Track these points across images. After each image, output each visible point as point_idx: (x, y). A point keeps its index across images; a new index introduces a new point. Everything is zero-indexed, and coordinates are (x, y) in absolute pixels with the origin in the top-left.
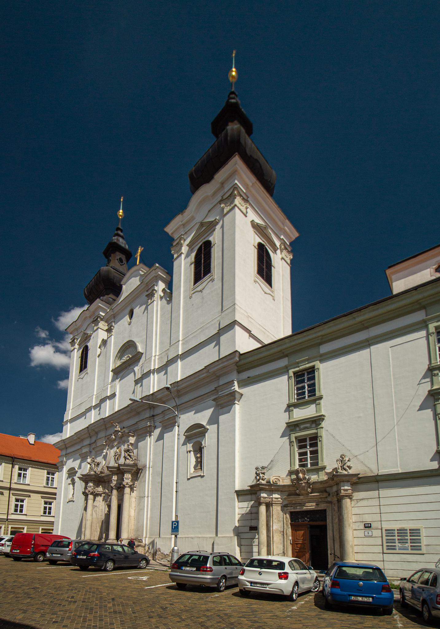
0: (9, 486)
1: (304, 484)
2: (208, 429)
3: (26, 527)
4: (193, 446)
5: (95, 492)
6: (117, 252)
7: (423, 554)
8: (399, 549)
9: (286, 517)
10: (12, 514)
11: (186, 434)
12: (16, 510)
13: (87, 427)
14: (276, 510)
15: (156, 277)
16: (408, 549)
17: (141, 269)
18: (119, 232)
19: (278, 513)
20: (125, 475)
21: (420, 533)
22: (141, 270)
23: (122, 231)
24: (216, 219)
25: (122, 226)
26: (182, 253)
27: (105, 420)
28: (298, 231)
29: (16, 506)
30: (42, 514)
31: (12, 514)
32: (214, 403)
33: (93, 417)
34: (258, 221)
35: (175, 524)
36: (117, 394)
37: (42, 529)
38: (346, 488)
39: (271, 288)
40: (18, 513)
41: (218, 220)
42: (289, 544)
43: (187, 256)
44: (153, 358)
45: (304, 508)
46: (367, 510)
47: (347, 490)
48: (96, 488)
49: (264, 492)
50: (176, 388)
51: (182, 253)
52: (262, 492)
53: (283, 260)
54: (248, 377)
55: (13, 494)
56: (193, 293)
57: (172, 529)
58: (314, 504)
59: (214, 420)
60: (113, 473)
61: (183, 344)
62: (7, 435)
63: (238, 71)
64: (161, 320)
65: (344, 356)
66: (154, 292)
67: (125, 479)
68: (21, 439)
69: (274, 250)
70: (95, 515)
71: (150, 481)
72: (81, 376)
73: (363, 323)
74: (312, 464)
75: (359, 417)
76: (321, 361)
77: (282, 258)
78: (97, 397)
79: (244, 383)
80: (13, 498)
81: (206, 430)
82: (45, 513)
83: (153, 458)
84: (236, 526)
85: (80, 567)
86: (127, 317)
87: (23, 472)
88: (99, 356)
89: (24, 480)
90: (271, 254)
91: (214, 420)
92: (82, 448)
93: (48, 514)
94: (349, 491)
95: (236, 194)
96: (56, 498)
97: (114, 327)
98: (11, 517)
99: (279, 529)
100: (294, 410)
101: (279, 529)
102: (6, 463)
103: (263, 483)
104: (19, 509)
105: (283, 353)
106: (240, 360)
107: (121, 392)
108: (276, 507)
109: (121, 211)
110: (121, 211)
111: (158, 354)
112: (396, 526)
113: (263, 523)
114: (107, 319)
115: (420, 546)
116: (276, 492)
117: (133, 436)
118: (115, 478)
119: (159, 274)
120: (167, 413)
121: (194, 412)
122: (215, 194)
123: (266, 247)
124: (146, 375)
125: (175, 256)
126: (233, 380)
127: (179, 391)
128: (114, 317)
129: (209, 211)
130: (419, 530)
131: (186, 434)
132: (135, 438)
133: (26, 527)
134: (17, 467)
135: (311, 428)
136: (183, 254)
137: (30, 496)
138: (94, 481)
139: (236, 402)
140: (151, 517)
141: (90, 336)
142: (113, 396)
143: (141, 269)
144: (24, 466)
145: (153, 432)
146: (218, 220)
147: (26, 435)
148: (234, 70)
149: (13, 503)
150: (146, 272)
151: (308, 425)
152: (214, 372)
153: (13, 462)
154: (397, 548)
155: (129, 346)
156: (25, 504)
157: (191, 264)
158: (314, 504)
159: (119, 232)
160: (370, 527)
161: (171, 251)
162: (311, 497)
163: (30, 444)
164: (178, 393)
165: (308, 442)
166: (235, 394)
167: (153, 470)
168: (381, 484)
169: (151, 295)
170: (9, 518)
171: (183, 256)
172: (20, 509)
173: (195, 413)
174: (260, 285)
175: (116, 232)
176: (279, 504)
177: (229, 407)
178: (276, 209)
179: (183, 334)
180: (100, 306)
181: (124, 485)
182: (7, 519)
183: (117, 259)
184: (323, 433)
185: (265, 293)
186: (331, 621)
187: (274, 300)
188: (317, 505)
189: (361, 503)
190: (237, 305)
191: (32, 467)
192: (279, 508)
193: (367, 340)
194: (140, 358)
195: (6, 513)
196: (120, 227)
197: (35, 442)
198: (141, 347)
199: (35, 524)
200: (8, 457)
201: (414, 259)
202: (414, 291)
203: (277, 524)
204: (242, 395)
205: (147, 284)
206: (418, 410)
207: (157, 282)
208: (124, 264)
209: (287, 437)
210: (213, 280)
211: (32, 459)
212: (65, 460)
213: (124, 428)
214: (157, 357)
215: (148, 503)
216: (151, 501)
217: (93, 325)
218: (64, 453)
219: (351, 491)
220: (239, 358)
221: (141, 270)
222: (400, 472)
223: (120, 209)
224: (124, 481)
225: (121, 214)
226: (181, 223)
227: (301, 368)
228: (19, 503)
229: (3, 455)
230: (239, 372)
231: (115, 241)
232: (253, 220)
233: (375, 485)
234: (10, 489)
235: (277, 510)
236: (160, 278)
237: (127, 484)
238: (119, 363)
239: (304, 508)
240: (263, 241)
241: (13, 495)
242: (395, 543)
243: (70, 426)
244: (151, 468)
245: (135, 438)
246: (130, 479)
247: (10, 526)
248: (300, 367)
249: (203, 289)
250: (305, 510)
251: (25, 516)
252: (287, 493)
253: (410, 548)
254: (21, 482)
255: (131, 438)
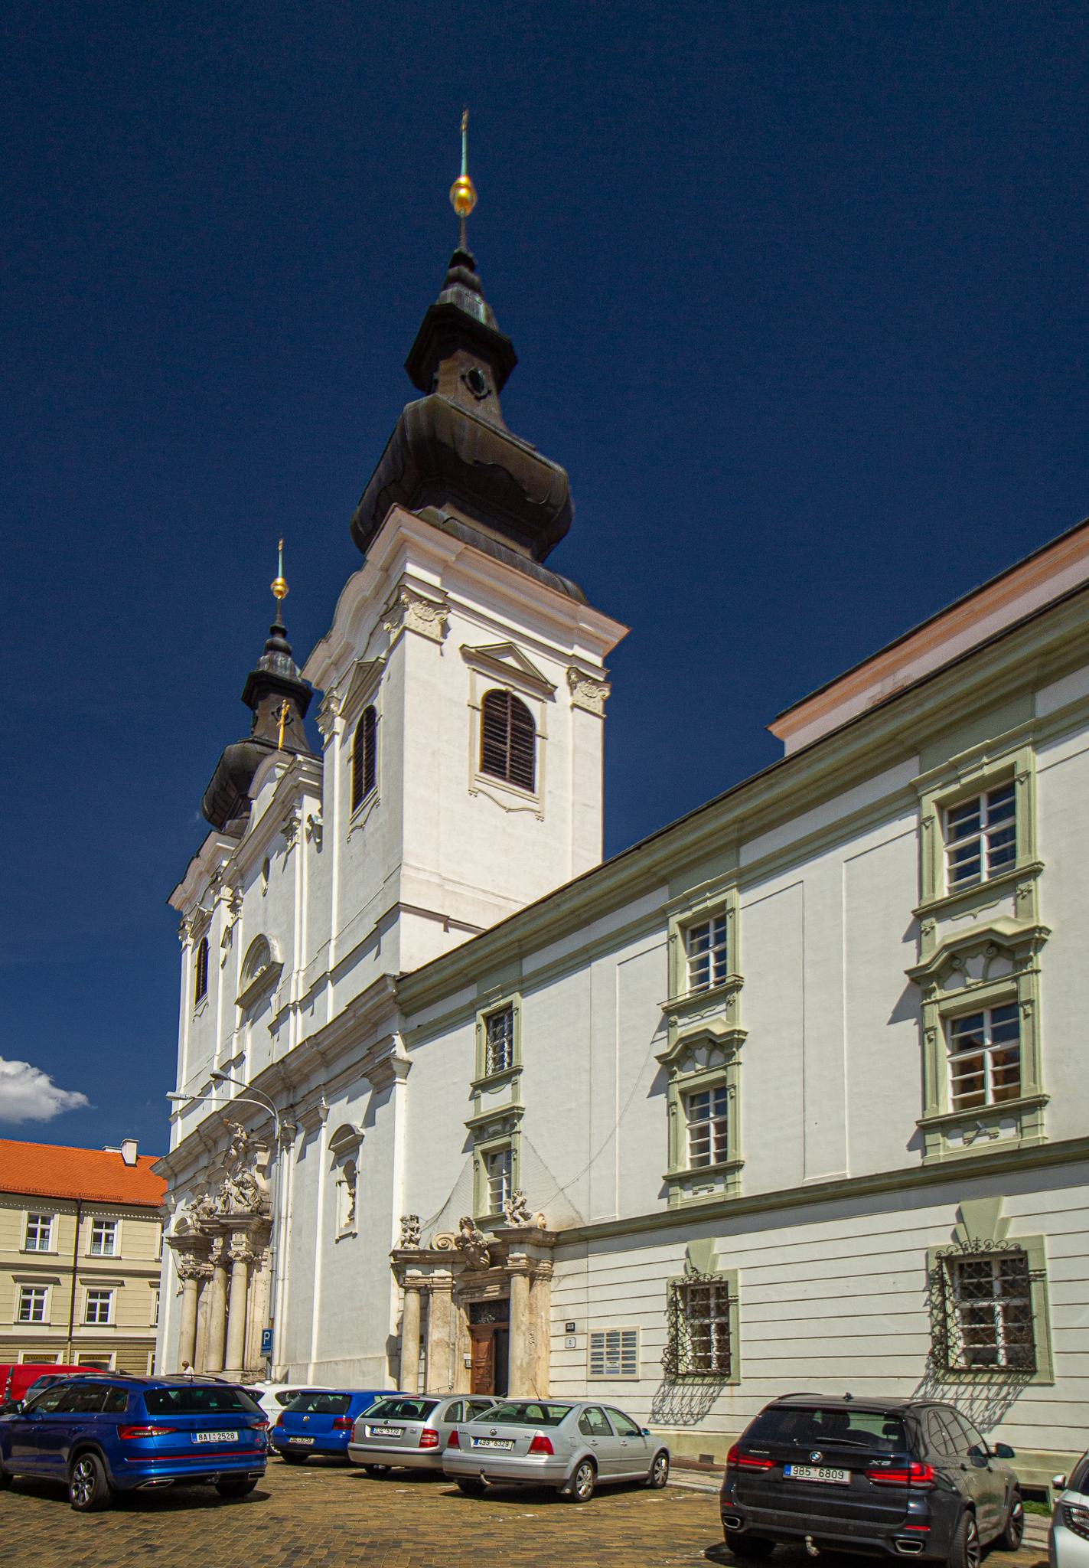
0: (72, 1265)
1: (472, 1249)
2: (363, 1136)
3: (114, 1355)
4: (344, 1171)
5: (198, 1273)
6: (271, 695)
7: (638, 1381)
8: (609, 1372)
9: (460, 1316)
10: (81, 1325)
11: (332, 1146)
12: (91, 1318)
13: (197, 1130)
14: (441, 1301)
15: (297, 787)
16: (618, 1372)
17: (279, 764)
18: (280, 640)
19: (445, 1307)
20: (234, 1236)
21: (634, 1339)
22: (278, 767)
23: (284, 633)
24: (378, 658)
25: (284, 620)
26: (334, 733)
27: (223, 1114)
28: (620, 620)
29: (92, 1307)
30: (15, 1318)
31: (81, 1325)
32: (366, 1080)
33: (214, 1104)
34: (484, 638)
35: (267, 1336)
36: (248, 1054)
37: (280, 1397)
38: (517, 1255)
39: (529, 793)
40: (97, 1322)
41: (384, 659)
42: (463, 1368)
43: (344, 741)
44: (294, 976)
45: (486, 1295)
46: (571, 1297)
47: (517, 1260)
48: (203, 1265)
49: (414, 1266)
50: (315, 1048)
51: (334, 733)
52: (409, 1266)
53: (576, 710)
54: (419, 1026)
55: (83, 1282)
56: (352, 831)
57: (263, 1345)
58: (497, 1287)
59: (370, 1120)
60: (215, 1233)
61: (336, 947)
62: (73, 1149)
63: (476, 184)
64: (309, 887)
65: (556, 982)
66: (295, 823)
67: (232, 1245)
68: (109, 1154)
69: (544, 694)
70: (204, 1322)
71: (288, 1246)
72: (199, 1012)
73: (577, 913)
74: (999, 1096)
75: (570, 1110)
76: (524, 993)
77: (574, 706)
78: (220, 1060)
79: (415, 1039)
80: (83, 1291)
81: (359, 1139)
82: (24, 1314)
83: (295, 1198)
84: (391, 1336)
85: (460, 1486)
86: (261, 876)
87: (104, 1231)
88: (223, 966)
89: (110, 1247)
90: (533, 705)
91: (370, 1120)
92: (197, 1175)
93: (100, 1321)
94: (522, 1261)
95: (406, 600)
96: (159, 1283)
97: (242, 900)
98: (78, 1332)
99: (446, 1339)
100: (482, 1095)
101: (446, 1339)
102: (62, 1213)
103: (412, 1249)
104: (97, 1313)
105: (466, 975)
106: (399, 992)
107: (254, 1050)
108: (440, 1294)
109: (280, 580)
110: (280, 580)
111: (304, 966)
112: (605, 1326)
113: (409, 1327)
114: (230, 881)
115: (634, 1365)
116: (442, 1265)
117: (266, 1150)
118: (218, 1242)
119: (301, 782)
120: (311, 1100)
121: (346, 1099)
122: (377, 591)
123: (517, 694)
124: (283, 1015)
125: (326, 738)
126: (390, 1035)
127: (324, 1053)
128: (242, 876)
129: (371, 635)
130: (634, 1333)
131: (332, 1146)
132: (269, 1153)
133: (114, 1355)
134: (89, 1221)
135: (504, 1133)
136: (338, 734)
137: (122, 1284)
138: (195, 1249)
139: (397, 1080)
140: (289, 1323)
141: (211, 917)
142: (241, 1058)
143: (279, 764)
144: (106, 1217)
145: (294, 1141)
146: (384, 659)
147: (119, 1144)
148: (463, 180)
149: (83, 1300)
150: (287, 766)
151: (498, 1127)
152: (366, 1016)
153: (79, 1210)
154: (605, 1369)
155: (260, 947)
156: (112, 1301)
157: (349, 761)
158: (497, 1287)
159: (280, 640)
160: (573, 1330)
161: (317, 727)
162: (494, 1274)
163: (126, 1165)
164: (324, 1058)
165: (987, 1027)
166: (391, 1064)
167: (293, 1223)
168: (593, 1245)
169: (290, 832)
170: (74, 1334)
171: (338, 739)
172: (101, 1315)
173: (348, 1102)
174: (489, 796)
175: (268, 641)
176: (448, 1288)
177: (388, 1090)
178: (540, 589)
179: (339, 924)
180: (220, 847)
181: (231, 1258)
182: (70, 1339)
183: (273, 713)
184: (520, 1143)
185: (509, 810)
186: (200, 1438)
187: (541, 819)
188: (501, 1288)
189: (568, 1283)
190: (407, 865)
191: (125, 1219)
192: (447, 1297)
193: (585, 950)
194: (280, 975)
195: (68, 1323)
196: (278, 624)
197: (138, 1158)
198: (280, 949)
199: (135, 1346)
200: (67, 1199)
201: (823, 695)
202: (637, 851)
203: (441, 1330)
204: (410, 1064)
205: (283, 802)
206: (649, 1097)
207: (301, 799)
208: (292, 720)
209: (664, 1095)
210: (377, 803)
211: (124, 1201)
212: (173, 1202)
213: (252, 1131)
214: (302, 974)
215: (283, 1290)
216: (291, 1292)
217: (212, 892)
218: (171, 1186)
219: (525, 1261)
220: (396, 987)
221: (278, 767)
222: (618, 1220)
223: (277, 577)
224: (212, 1252)
225: (279, 588)
226: (328, 661)
227: (494, 1006)
228: (99, 1301)
229: (51, 1197)
230: (407, 1015)
231: (266, 667)
232: (464, 646)
233: (580, 1248)
234: (75, 1270)
235: (443, 1301)
236: (304, 788)
237: (238, 1255)
238: (249, 983)
239: (486, 1295)
240: (505, 684)
241: (82, 1284)
242: (602, 1359)
243: (183, 1124)
244: (289, 1219)
245: (269, 1153)
246: (244, 1245)
247: (77, 1354)
248: (493, 1006)
249: (365, 822)
250: (487, 1299)
251: (113, 1329)
252: (463, 1267)
253: (621, 1369)
254: (102, 1254)
255: (259, 1153)
